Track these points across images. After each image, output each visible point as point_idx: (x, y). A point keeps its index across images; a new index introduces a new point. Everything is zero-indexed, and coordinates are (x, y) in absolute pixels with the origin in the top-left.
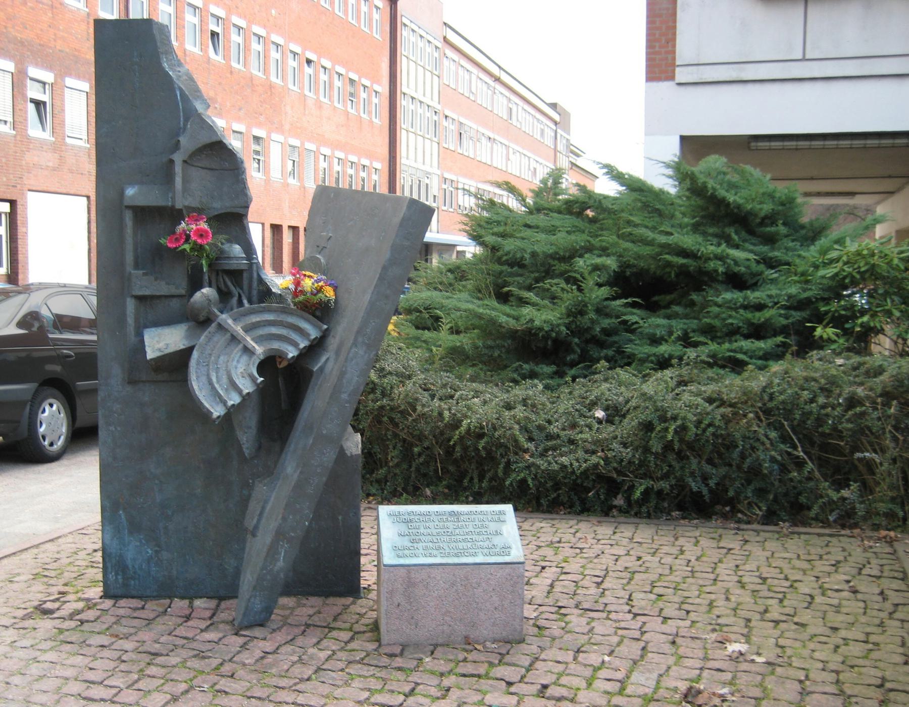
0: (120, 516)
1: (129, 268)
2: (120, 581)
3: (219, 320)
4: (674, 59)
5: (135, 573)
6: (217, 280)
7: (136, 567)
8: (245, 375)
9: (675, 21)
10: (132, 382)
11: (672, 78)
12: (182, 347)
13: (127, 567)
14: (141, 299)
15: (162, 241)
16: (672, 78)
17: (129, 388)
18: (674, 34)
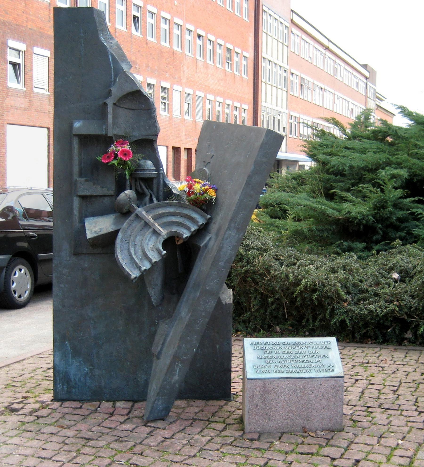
3: (136, 212)
8: (154, 249)
10: (76, 254)
12: (111, 230)
14: (83, 198)
15: (99, 158)
17: (74, 258)
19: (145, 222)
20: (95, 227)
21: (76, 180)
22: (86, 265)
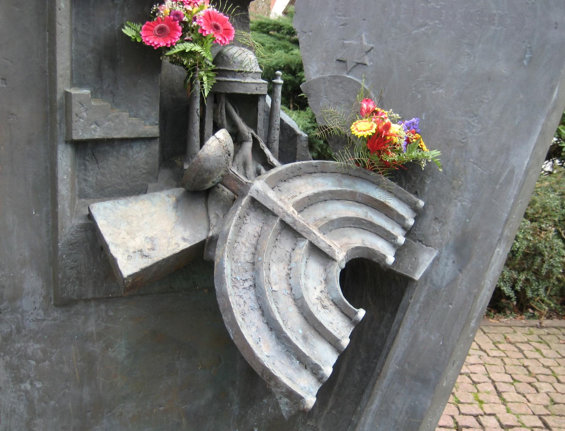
1: (63, 85)
3: (252, 193)
6: (215, 112)
8: (327, 303)
10: (64, 303)
12: (184, 245)
14: (85, 149)
15: (128, 32)
17: (56, 314)
19: (283, 222)
20: (132, 234)
21: (67, 95)
22: (91, 327)
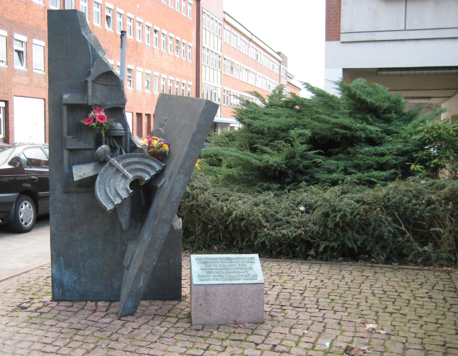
0: (60, 260)
2: (61, 292)
3: (110, 161)
4: (340, 30)
5: (68, 288)
7: (69, 285)
8: (124, 189)
9: (340, 11)
10: (66, 192)
11: (338, 39)
12: (92, 175)
13: (64, 286)
14: (71, 150)
15: (82, 121)
16: (338, 39)
17: (65, 196)
18: (340, 17)
19: (117, 169)
20: (80, 172)
